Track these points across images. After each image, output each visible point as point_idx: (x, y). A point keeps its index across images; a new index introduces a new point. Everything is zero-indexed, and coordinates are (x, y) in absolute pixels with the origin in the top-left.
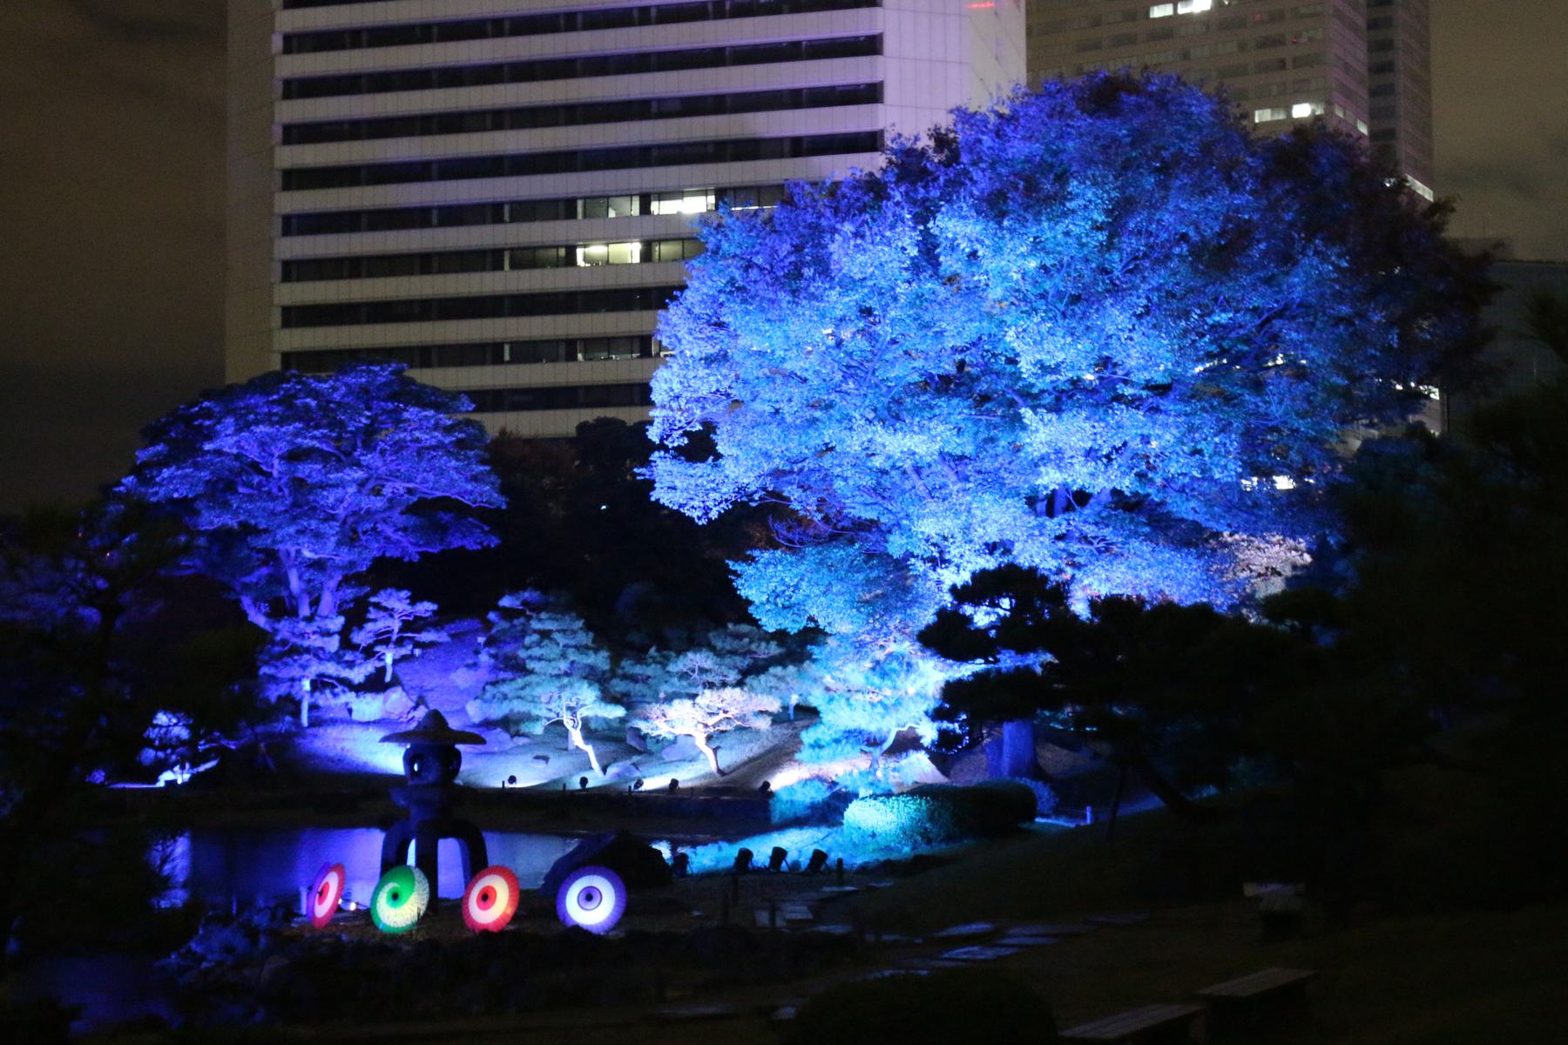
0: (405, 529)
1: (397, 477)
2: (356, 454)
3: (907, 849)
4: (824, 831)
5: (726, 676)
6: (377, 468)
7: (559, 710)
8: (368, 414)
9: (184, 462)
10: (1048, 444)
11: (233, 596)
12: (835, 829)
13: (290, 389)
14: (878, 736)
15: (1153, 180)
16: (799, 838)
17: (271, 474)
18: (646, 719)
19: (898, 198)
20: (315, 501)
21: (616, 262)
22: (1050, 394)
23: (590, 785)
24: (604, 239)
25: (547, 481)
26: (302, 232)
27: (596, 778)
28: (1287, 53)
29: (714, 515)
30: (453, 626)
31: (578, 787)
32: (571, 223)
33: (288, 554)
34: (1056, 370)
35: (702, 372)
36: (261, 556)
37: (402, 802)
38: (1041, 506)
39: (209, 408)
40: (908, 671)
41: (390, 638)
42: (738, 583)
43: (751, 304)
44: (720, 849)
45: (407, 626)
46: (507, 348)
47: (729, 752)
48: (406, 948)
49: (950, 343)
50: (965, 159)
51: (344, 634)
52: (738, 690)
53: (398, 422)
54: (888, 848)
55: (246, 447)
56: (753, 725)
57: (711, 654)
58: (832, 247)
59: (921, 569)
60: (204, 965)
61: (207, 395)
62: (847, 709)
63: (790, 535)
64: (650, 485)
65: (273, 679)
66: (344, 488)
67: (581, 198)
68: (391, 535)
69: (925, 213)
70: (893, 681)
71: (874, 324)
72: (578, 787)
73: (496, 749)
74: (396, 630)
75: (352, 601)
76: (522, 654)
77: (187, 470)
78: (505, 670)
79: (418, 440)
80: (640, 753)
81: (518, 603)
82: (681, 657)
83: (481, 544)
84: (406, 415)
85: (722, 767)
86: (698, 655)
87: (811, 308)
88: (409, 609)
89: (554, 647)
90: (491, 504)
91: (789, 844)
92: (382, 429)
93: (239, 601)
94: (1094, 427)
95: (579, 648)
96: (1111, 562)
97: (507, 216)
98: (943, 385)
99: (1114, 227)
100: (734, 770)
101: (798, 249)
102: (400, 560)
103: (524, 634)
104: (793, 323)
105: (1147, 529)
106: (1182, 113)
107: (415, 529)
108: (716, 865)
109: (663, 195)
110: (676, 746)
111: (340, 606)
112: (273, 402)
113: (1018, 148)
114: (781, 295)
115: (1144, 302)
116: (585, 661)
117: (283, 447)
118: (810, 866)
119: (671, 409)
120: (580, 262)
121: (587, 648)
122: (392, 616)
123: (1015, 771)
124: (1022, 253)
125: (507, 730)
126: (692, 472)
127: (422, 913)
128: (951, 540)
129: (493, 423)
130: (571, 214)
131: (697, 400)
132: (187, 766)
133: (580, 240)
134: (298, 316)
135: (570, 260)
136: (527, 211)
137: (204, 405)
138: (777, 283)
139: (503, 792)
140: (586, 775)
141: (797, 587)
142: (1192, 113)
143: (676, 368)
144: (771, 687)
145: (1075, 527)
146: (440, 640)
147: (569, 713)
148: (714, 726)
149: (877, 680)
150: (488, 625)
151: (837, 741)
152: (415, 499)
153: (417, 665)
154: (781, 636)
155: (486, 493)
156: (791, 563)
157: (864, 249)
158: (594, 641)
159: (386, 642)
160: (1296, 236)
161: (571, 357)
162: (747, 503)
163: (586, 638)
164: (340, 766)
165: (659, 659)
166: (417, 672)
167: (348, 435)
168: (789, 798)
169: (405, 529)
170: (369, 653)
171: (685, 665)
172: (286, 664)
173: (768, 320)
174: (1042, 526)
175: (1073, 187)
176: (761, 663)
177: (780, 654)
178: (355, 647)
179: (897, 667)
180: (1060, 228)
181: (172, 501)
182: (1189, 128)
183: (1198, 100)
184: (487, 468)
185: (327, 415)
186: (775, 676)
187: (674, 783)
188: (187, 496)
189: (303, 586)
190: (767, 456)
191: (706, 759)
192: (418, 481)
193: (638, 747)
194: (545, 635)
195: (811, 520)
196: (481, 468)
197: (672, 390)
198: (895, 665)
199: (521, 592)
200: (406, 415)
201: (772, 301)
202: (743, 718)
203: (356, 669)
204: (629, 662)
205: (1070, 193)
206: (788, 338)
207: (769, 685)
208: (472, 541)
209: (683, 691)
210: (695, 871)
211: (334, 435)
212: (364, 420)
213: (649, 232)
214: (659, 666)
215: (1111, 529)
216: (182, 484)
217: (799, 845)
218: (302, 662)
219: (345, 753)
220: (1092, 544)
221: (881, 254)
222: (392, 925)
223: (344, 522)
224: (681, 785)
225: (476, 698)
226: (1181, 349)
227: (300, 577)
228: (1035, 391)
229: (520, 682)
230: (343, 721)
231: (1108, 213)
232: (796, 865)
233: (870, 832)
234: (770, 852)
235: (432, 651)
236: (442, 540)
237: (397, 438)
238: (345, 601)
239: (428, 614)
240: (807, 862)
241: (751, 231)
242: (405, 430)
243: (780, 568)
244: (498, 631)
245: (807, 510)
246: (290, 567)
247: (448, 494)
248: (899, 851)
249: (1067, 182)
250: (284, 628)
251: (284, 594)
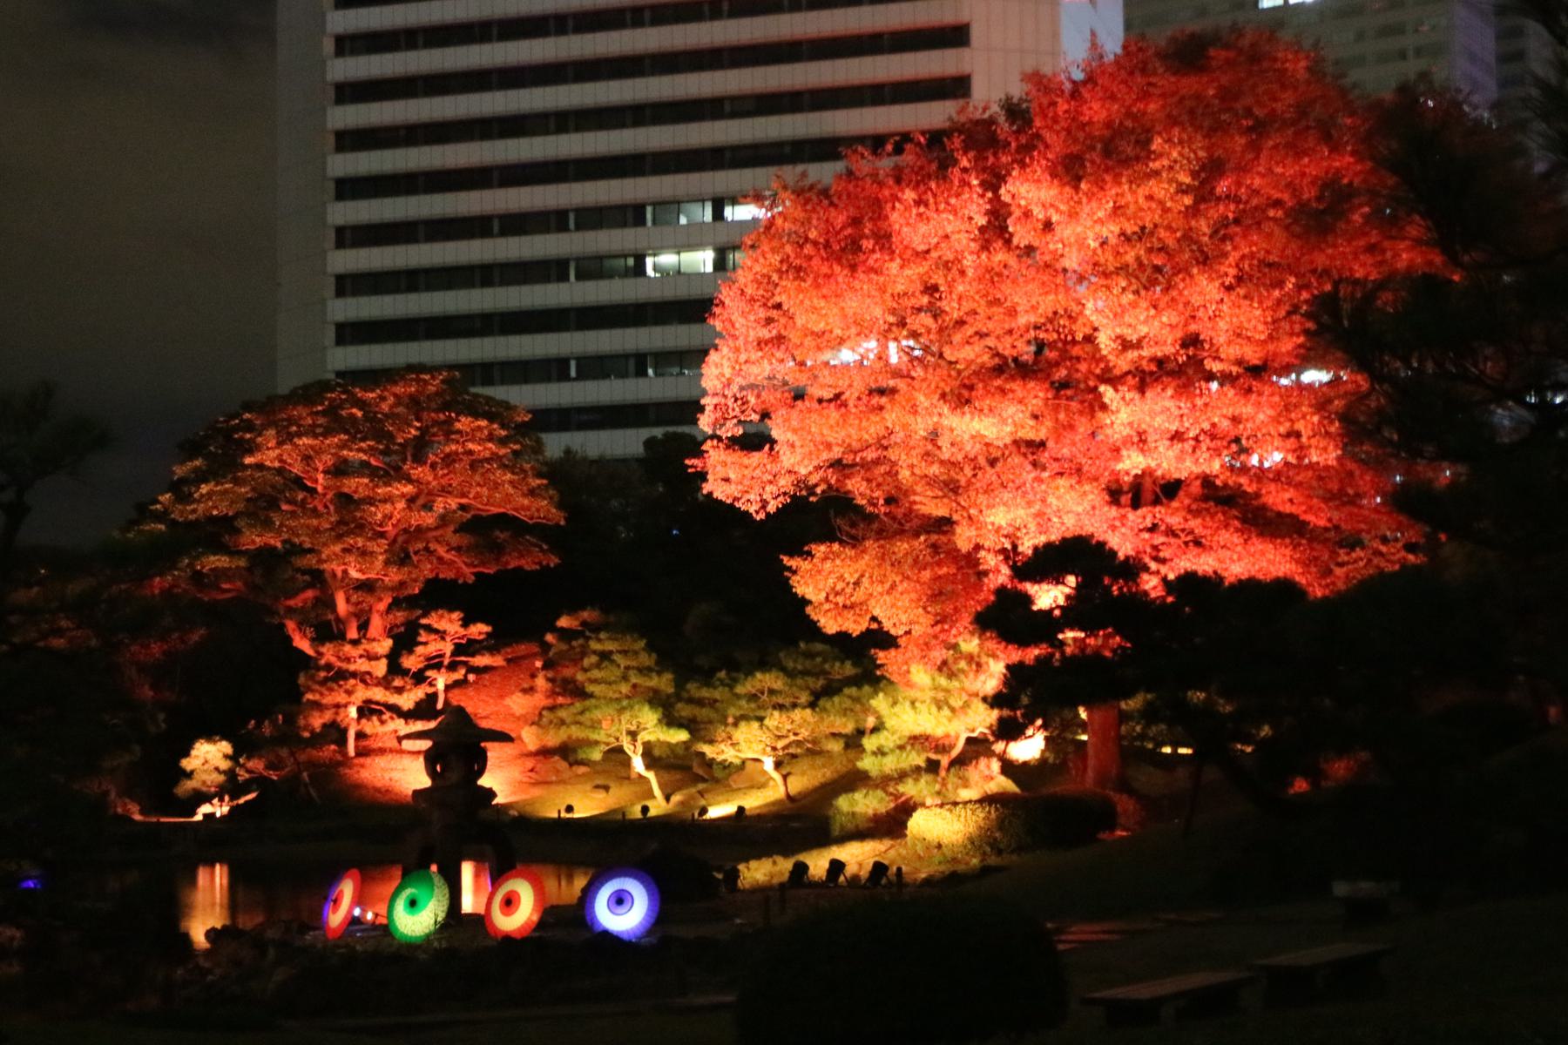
0: (458, 549)
1: (449, 493)
2: (405, 467)
3: (975, 861)
4: (887, 843)
6: (428, 483)
8: (418, 425)
10: (1131, 424)
11: (276, 621)
14: (947, 743)
17: (315, 490)
18: (711, 742)
19: (965, 163)
20: (361, 518)
21: (689, 270)
22: (1134, 376)
28: (1409, 41)
29: (772, 508)
30: (509, 650)
31: (639, 815)
32: (640, 230)
33: (334, 575)
34: (1138, 345)
36: (307, 578)
38: (1125, 499)
39: (248, 420)
41: (442, 662)
42: (794, 581)
44: (775, 863)
45: (459, 649)
46: (573, 364)
47: (800, 778)
48: (423, 956)
49: (1023, 320)
50: (1038, 123)
51: (393, 658)
52: (808, 711)
53: (448, 431)
54: (954, 860)
55: (289, 461)
57: (781, 674)
58: (894, 216)
59: (992, 563)
60: (210, 978)
61: (248, 407)
63: (853, 532)
64: (702, 476)
65: (318, 706)
66: (393, 504)
69: (994, 181)
70: (961, 682)
72: (639, 815)
73: (554, 778)
74: (448, 654)
75: (402, 624)
76: (580, 677)
77: (227, 486)
79: (471, 452)
80: (704, 780)
83: (540, 563)
84: (458, 426)
86: (767, 676)
87: (870, 281)
88: (462, 631)
92: (433, 442)
93: (282, 626)
94: (1180, 408)
95: (642, 671)
97: (572, 225)
99: (1203, 194)
102: (454, 581)
103: (584, 653)
107: (469, 548)
109: (734, 201)
110: (744, 772)
111: (391, 630)
112: (318, 413)
113: (1096, 111)
114: (837, 269)
117: (328, 459)
119: (725, 396)
120: (650, 272)
121: (650, 669)
122: (443, 639)
124: (1100, 219)
125: (565, 757)
126: (746, 461)
127: (439, 919)
128: (1024, 531)
129: (555, 444)
130: (640, 221)
132: (227, 798)
133: (650, 248)
134: (351, 333)
135: (640, 270)
136: (594, 218)
139: (559, 823)
140: (649, 803)
141: (857, 583)
142: (1286, 69)
144: (846, 709)
145: (1161, 520)
147: (629, 738)
148: (784, 748)
150: (546, 647)
151: (901, 748)
152: (469, 516)
153: (471, 691)
155: (543, 509)
156: (851, 558)
158: (657, 663)
161: (642, 373)
162: (807, 498)
163: (647, 660)
164: (387, 798)
165: (727, 681)
168: (851, 810)
170: (419, 678)
172: (331, 690)
173: (824, 297)
175: (1157, 144)
177: (856, 675)
178: (404, 673)
180: (1142, 192)
181: (212, 520)
182: (1283, 87)
184: (545, 482)
185: (375, 428)
186: (850, 697)
187: (741, 809)
189: (352, 609)
190: (829, 446)
191: (777, 785)
192: (471, 496)
194: (605, 656)
196: (538, 482)
198: (963, 664)
200: (458, 426)
202: (815, 742)
203: (405, 695)
206: (845, 316)
207: (844, 706)
208: (531, 559)
210: (747, 886)
212: (413, 432)
213: (722, 239)
216: (222, 500)
217: (860, 858)
219: (393, 783)
223: (395, 541)
226: (1274, 322)
227: (348, 601)
228: (1117, 372)
229: (578, 706)
230: (391, 751)
232: (856, 878)
233: (935, 843)
234: (827, 865)
235: (487, 676)
237: (447, 450)
239: (482, 637)
240: (867, 875)
242: (458, 442)
247: (502, 510)
248: (967, 864)
249: (1149, 141)
250: (328, 653)
251: (331, 617)
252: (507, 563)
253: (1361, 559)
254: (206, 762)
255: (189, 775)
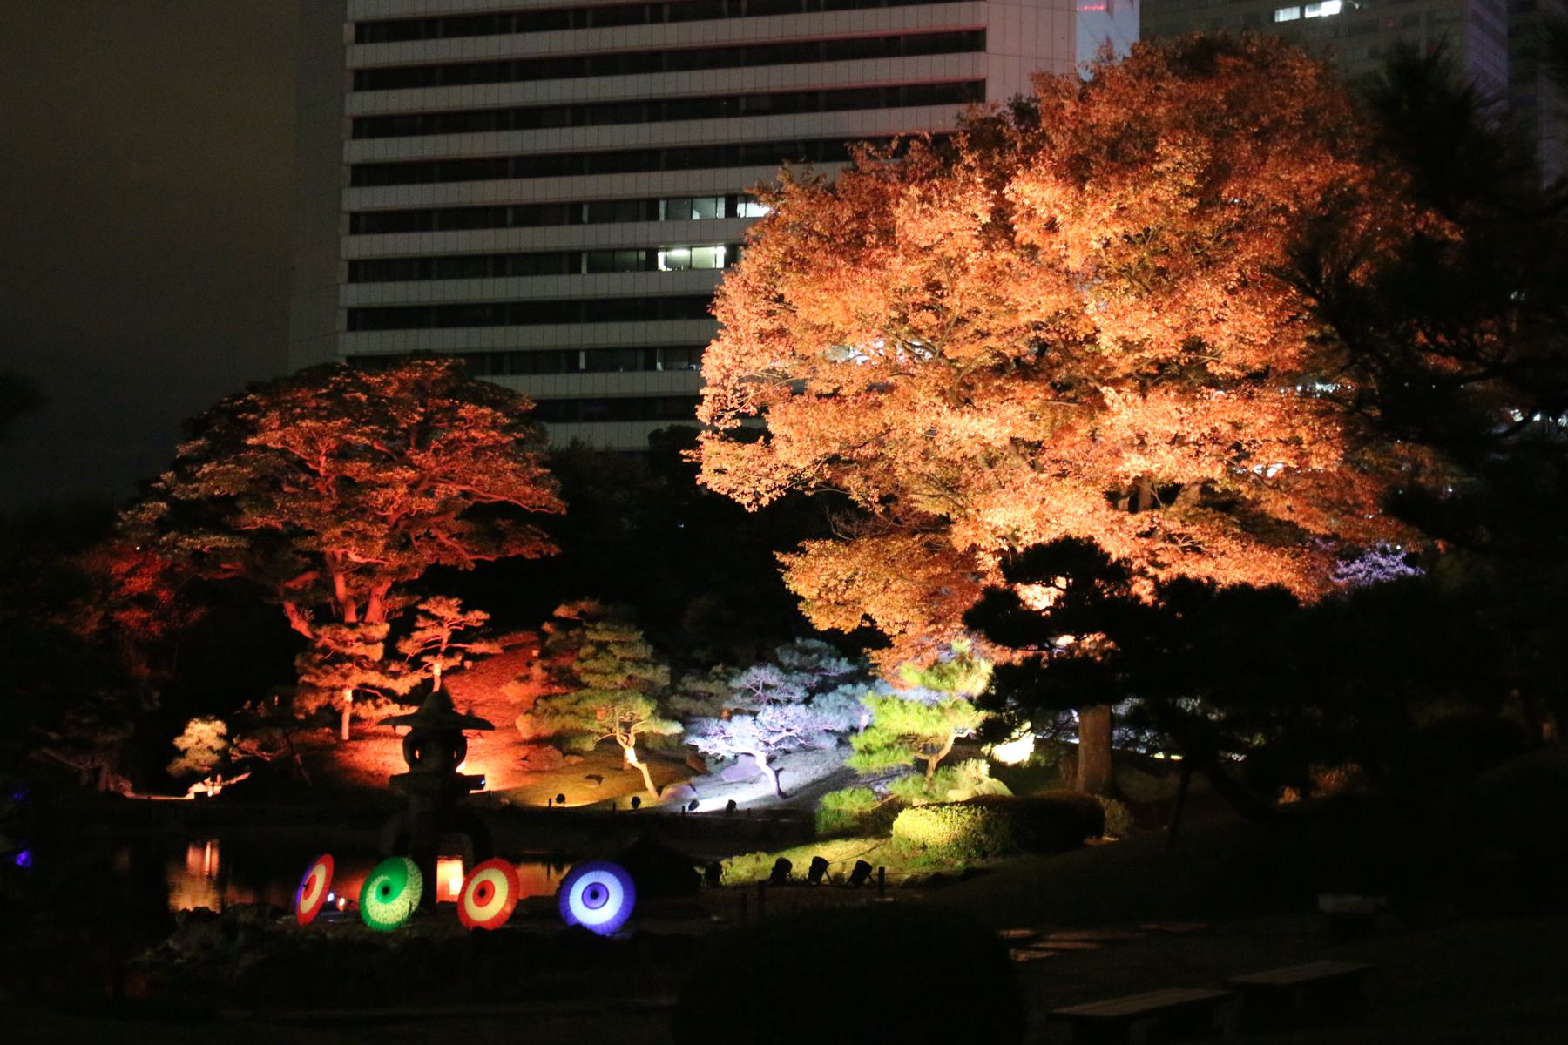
0: (460, 536)
1: (452, 480)
4: (872, 842)
5: (792, 694)
6: (431, 469)
7: (612, 725)
8: (422, 410)
9: (226, 457)
12: (884, 841)
13: (339, 382)
15: (1249, 147)
16: (844, 849)
18: (704, 735)
21: (700, 266)
23: (644, 804)
24: (687, 242)
25: (619, 495)
26: (371, 230)
27: (649, 799)
29: (765, 502)
30: (507, 638)
31: (630, 807)
33: (334, 558)
34: (1140, 347)
35: (756, 347)
37: (401, 792)
38: (1123, 503)
40: (968, 671)
41: (439, 648)
42: (786, 577)
43: (807, 273)
44: (758, 859)
45: (456, 636)
46: (582, 355)
48: (393, 946)
51: (390, 642)
52: (802, 707)
53: (453, 418)
56: (817, 745)
57: (777, 670)
58: (898, 212)
61: (253, 388)
62: (901, 711)
64: (696, 468)
65: (313, 688)
66: (394, 488)
67: (664, 199)
68: (445, 541)
69: (998, 180)
71: (942, 296)
72: (630, 807)
73: (547, 767)
74: (445, 641)
75: (401, 610)
76: (576, 667)
77: (230, 466)
78: (558, 683)
79: (474, 440)
81: (575, 613)
82: (745, 673)
83: (540, 552)
84: (462, 413)
85: (784, 788)
88: (460, 618)
89: (610, 659)
90: (549, 509)
91: (833, 856)
93: (282, 607)
95: (638, 662)
96: (1198, 561)
97: (585, 218)
98: (1024, 371)
99: (1207, 195)
100: (796, 793)
101: (860, 217)
102: (454, 568)
103: (581, 643)
104: (853, 293)
105: (1237, 531)
106: (1284, 77)
107: (470, 536)
108: (752, 877)
109: (748, 199)
110: (737, 766)
111: (389, 614)
112: (322, 396)
115: (1237, 275)
116: (643, 676)
117: (331, 442)
118: (852, 878)
120: (661, 266)
121: (646, 661)
123: (1091, 787)
126: (739, 451)
130: (653, 216)
131: (751, 378)
132: (219, 778)
135: (652, 263)
136: (607, 211)
137: (249, 398)
138: (838, 251)
139: (549, 811)
140: (640, 795)
142: (1295, 77)
143: (727, 341)
144: (840, 707)
146: (492, 652)
149: (933, 681)
151: (889, 747)
152: (471, 503)
153: (467, 678)
154: (833, 635)
155: (545, 497)
156: (845, 556)
157: (931, 215)
158: (653, 655)
159: (435, 652)
160: (1405, 207)
163: (644, 651)
165: (722, 675)
166: (467, 685)
167: (399, 432)
169: (460, 536)
170: (416, 663)
171: (748, 681)
172: (327, 673)
174: (1121, 521)
176: (832, 681)
177: (852, 673)
178: (401, 657)
179: (956, 668)
180: (1148, 192)
182: (1292, 93)
183: (1301, 62)
184: (548, 471)
185: (377, 412)
186: (845, 694)
187: (732, 804)
188: (228, 494)
190: (824, 440)
192: (473, 483)
193: (697, 769)
194: (602, 647)
195: (873, 513)
196: (541, 471)
197: (724, 367)
199: (578, 602)
200: (462, 413)
201: (830, 270)
202: (807, 738)
203: (401, 680)
204: (691, 678)
205: (1158, 154)
208: (532, 548)
209: (746, 709)
210: (729, 882)
211: (384, 431)
212: (417, 417)
213: (733, 236)
214: (722, 683)
215: (1198, 527)
217: (844, 857)
218: (343, 670)
219: (386, 768)
220: (1175, 542)
221: (949, 220)
222: (381, 921)
223: (396, 525)
224: (738, 807)
225: (526, 713)
227: (347, 584)
229: (573, 695)
231: (1199, 178)
233: (920, 844)
234: (810, 863)
236: (498, 548)
237: (451, 436)
238: (395, 610)
239: (479, 624)
240: (850, 874)
241: (811, 198)
243: (831, 559)
244: (552, 643)
245: (867, 502)
246: (337, 571)
250: (326, 635)
252: (508, 551)
253: (1360, 571)
254: (200, 741)
255: (183, 753)
